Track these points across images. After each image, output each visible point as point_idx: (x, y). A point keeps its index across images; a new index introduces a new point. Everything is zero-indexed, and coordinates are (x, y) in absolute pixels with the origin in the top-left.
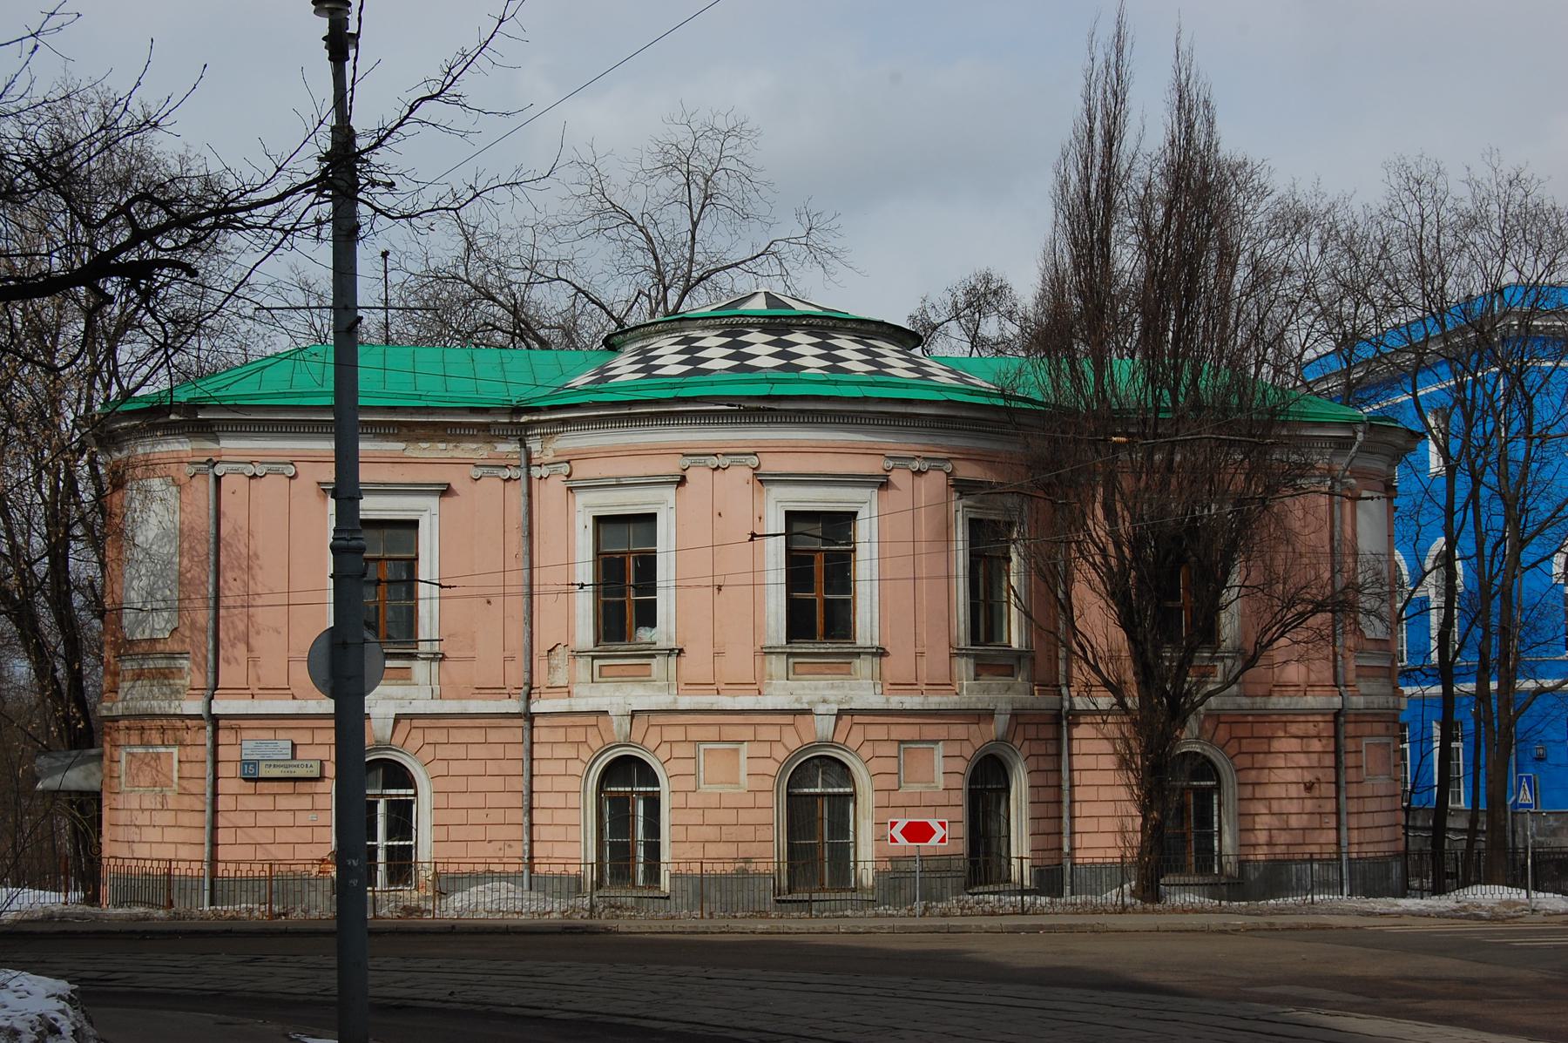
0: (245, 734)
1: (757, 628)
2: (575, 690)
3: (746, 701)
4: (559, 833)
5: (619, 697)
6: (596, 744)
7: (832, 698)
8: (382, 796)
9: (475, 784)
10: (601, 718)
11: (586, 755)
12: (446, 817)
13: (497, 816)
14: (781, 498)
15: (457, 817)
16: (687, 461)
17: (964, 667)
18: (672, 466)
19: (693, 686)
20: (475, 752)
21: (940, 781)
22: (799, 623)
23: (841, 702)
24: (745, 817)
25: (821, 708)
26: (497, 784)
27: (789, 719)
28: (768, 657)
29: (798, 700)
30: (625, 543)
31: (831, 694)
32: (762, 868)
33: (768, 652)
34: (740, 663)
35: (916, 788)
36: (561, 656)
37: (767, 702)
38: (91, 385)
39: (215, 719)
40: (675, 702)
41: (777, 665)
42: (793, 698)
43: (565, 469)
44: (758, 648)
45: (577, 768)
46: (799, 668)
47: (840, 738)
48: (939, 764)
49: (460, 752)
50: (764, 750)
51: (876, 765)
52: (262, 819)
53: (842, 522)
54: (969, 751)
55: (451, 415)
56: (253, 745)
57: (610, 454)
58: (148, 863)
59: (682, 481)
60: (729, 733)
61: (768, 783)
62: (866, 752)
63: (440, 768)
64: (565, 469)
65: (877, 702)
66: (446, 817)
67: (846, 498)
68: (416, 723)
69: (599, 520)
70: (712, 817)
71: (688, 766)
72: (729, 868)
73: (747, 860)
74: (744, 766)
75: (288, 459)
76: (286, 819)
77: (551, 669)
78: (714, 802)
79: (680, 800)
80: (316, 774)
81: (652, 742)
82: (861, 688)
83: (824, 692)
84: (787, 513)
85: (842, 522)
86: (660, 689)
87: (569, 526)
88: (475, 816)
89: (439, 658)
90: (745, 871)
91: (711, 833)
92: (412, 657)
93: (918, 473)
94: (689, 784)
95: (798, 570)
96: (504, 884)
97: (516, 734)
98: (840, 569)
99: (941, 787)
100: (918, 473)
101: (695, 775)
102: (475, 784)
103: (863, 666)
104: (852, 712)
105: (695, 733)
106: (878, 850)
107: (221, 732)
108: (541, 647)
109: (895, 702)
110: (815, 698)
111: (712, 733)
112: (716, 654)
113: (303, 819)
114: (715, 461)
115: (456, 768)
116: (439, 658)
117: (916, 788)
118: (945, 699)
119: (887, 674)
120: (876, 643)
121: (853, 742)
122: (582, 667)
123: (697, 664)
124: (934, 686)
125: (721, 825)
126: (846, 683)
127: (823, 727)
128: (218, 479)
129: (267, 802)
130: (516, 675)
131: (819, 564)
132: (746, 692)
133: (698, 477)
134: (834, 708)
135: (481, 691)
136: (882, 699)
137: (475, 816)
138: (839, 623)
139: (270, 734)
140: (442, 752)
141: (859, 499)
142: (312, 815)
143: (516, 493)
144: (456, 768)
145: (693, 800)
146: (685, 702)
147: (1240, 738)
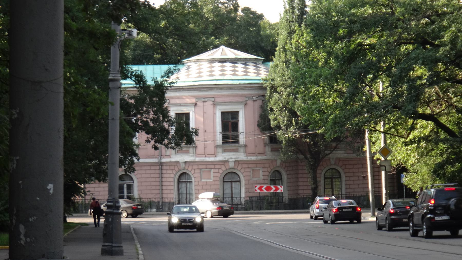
2: (172, 156)
3: (212, 159)
4: (169, 192)
10: (226, 164)
11: (174, 172)
12: (349, 182)
13: (153, 188)
16: (247, 99)
17: (268, 149)
18: (194, 101)
19: (200, 155)
20: (148, 172)
21: (262, 177)
22: (225, 138)
23: (235, 159)
25: (231, 160)
26: (153, 180)
29: (225, 158)
31: (233, 157)
33: (217, 147)
34: (211, 149)
35: (255, 179)
37: (217, 159)
38: (448, 80)
39: (161, 164)
41: (220, 150)
45: (172, 175)
47: (236, 167)
48: (261, 173)
49: (144, 172)
50: (217, 171)
51: (245, 174)
52: (356, 182)
53: (235, 115)
54: (269, 170)
57: (179, 98)
59: (196, 105)
61: (218, 179)
62: (242, 171)
63: (139, 176)
66: (349, 182)
71: (199, 175)
74: (212, 175)
78: (205, 184)
79: (197, 183)
81: (190, 169)
82: (241, 156)
83: (231, 157)
85: (187, 115)
86: (192, 156)
93: (204, 102)
94: (199, 179)
95: (225, 126)
98: (235, 126)
99: (262, 178)
100: (204, 102)
101: (201, 177)
103: (242, 150)
106: (246, 195)
109: (249, 158)
114: (204, 100)
115: (143, 176)
117: (255, 179)
124: (260, 154)
131: (230, 124)
132: (212, 157)
133: (200, 104)
134: (234, 160)
138: (235, 140)
144: (143, 176)
146: (198, 159)
147: (195, 169)
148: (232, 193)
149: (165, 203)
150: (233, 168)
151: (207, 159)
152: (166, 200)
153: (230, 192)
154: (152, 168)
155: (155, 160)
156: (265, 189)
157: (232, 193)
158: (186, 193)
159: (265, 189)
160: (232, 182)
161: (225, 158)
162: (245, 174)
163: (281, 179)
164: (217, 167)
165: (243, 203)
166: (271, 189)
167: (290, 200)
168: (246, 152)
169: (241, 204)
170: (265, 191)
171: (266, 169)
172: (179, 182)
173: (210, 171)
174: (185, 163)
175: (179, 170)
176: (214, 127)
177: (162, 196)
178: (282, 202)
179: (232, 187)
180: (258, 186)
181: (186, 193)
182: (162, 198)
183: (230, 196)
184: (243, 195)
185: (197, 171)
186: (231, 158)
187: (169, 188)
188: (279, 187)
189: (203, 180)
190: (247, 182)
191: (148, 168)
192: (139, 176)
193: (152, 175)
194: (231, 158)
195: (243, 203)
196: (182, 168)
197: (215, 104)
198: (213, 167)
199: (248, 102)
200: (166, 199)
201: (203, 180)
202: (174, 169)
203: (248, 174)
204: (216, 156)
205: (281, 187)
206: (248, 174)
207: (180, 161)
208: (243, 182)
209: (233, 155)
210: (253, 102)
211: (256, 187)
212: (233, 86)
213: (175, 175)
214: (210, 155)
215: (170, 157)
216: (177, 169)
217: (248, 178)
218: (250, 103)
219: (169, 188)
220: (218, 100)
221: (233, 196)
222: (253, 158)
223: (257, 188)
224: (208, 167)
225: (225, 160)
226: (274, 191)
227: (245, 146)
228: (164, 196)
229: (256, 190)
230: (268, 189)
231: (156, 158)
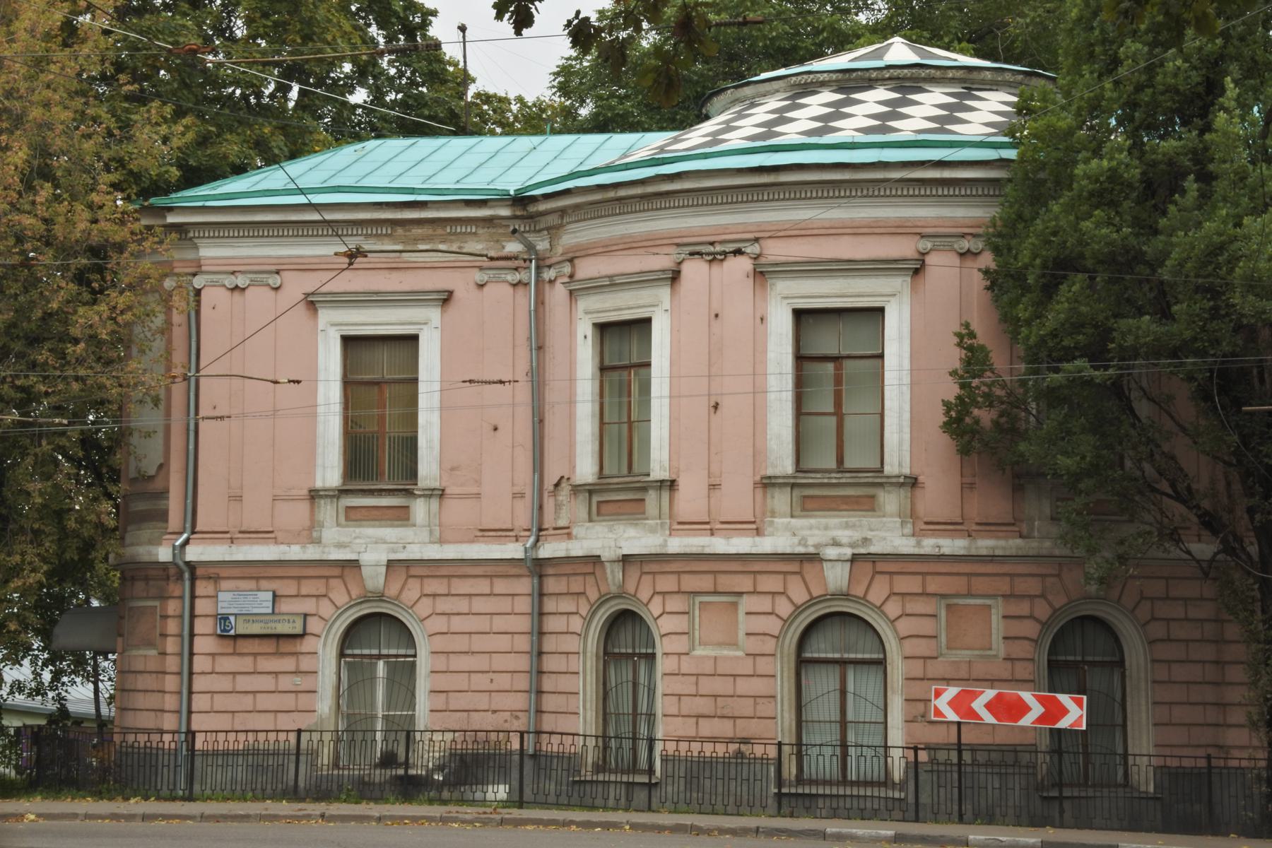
0: (225, 584)
1: (758, 453)
3: (741, 544)
5: (373, 546)
6: (800, 596)
7: (845, 540)
8: (379, 657)
9: (479, 643)
10: (808, 567)
11: (785, 609)
14: (786, 292)
15: (460, 682)
16: (926, 245)
20: (480, 605)
21: (999, 647)
23: (851, 545)
24: (744, 686)
25: (831, 553)
27: (794, 567)
28: (769, 491)
30: (383, 365)
31: (844, 535)
32: (759, 750)
33: (768, 484)
34: (738, 497)
36: (565, 489)
37: (766, 545)
40: (665, 544)
42: (796, 540)
43: (567, 269)
44: (758, 478)
46: (604, 508)
47: (859, 591)
50: (764, 604)
51: (905, 626)
54: (1043, 611)
55: (438, 209)
56: (230, 599)
58: (261, 737)
60: (726, 582)
62: (893, 609)
64: (567, 269)
65: (905, 545)
67: (868, 290)
68: (881, 566)
69: (603, 329)
70: (707, 686)
72: (721, 749)
73: (745, 741)
75: (273, 268)
76: (266, 683)
77: (558, 507)
78: (708, 668)
80: (299, 630)
83: (834, 534)
84: (595, 325)
86: (653, 531)
87: (572, 334)
88: (481, 681)
89: (441, 494)
90: (739, 754)
91: (704, 705)
92: (409, 493)
96: (1105, 790)
97: (525, 585)
99: (1002, 654)
102: (479, 643)
103: (890, 501)
104: (408, 564)
105: (690, 583)
106: (909, 733)
107: (198, 583)
108: (549, 483)
109: (929, 545)
110: (823, 540)
111: (705, 583)
112: (713, 487)
113: (286, 682)
115: (458, 624)
116: (314, 495)
118: (1002, 543)
119: (921, 509)
120: (907, 471)
121: (876, 596)
122: (579, 508)
123: (690, 499)
125: (715, 696)
126: (865, 521)
127: (836, 576)
128: (198, 292)
129: (246, 663)
130: (523, 516)
133: (694, 270)
134: (848, 552)
135: (487, 533)
136: (912, 541)
137: (481, 681)
139: (252, 584)
140: (444, 605)
141: (888, 290)
142: (298, 680)
143: (525, 300)
144: (458, 624)
145: (687, 666)
146: (676, 545)
148: (844, 723)
149: (550, 757)
150: (845, 596)
151: (719, 545)
152: (552, 745)
153: (836, 716)
154: (501, 586)
155: (513, 550)
156: (988, 706)
157: (844, 723)
158: (635, 714)
159: (988, 706)
160: (843, 663)
161: (803, 542)
162: (905, 626)
163: (1121, 663)
164: (770, 583)
165: (897, 774)
166: (1024, 709)
167: (1169, 776)
168: (913, 514)
169: (886, 782)
170: (989, 718)
171: (1023, 608)
172: (609, 656)
173: (735, 605)
174: (626, 560)
175: (604, 600)
176: (759, 391)
177: (538, 721)
178: (1126, 783)
179: (843, 692)
180: (952, 692)
181: (635, 714)
182: (538, 733)
183: (835, 737)
184: (897, 736)
185: (675, 604)
186: (836, 543)
187: (564, 683)
188: (1064, 699)
189: (699, 652)
190: (917, 669)
191: (483, 586)
192: (439, 624)
193: (500, 623)
194: (836, 543)
195: (897, 774)
196: (614, 589)
197: (762, 274)
198: (745, 583)
199: (929, 260)
200: (556, 739)
201: (699, 652)
202: (584, 593)
203: (926, 626)
204: (759, 532)
205: (1079, 703)
206: (926, 626)
207: (606, 555)
208: (897, 669)
209: (847, 526)
210: (956, 260)
211: (938, 694)
212: (846, 175)
213: (588, 621)
214: (734, 526)
215: (569, 536)
216: (593, 595)
217: (922, 647)
218: (942, 266)
219: (564, 683)
220: (776, 251)
221: (851, 738)
222: (952, 545)
223: (942, 703)
224: (726, 582)
225: (801, 550)
226: (1040, 719)
227: (912, 482)
228: (548, 723)
229: (938, 712)
230: (1009, 709)
231: (517, 539)
